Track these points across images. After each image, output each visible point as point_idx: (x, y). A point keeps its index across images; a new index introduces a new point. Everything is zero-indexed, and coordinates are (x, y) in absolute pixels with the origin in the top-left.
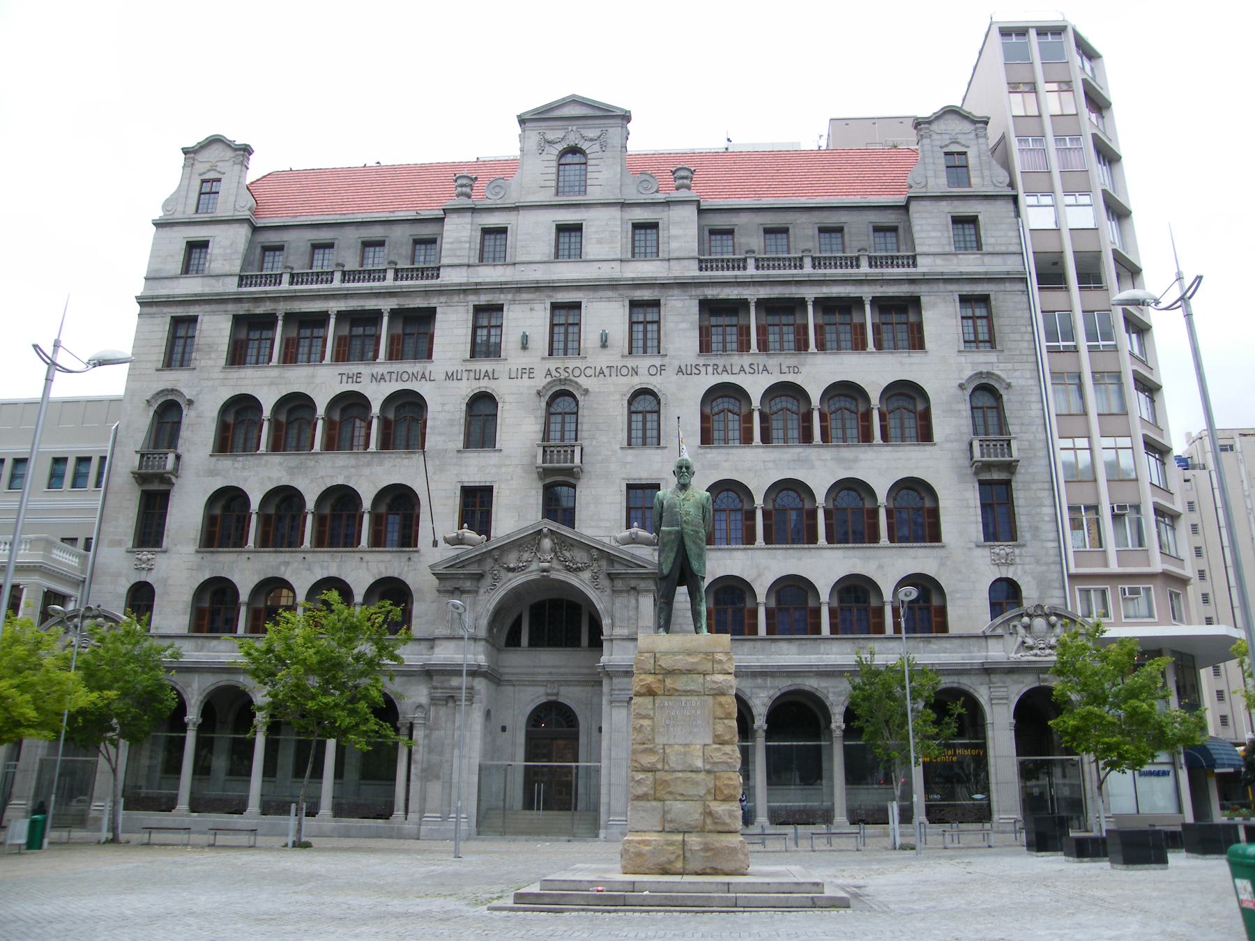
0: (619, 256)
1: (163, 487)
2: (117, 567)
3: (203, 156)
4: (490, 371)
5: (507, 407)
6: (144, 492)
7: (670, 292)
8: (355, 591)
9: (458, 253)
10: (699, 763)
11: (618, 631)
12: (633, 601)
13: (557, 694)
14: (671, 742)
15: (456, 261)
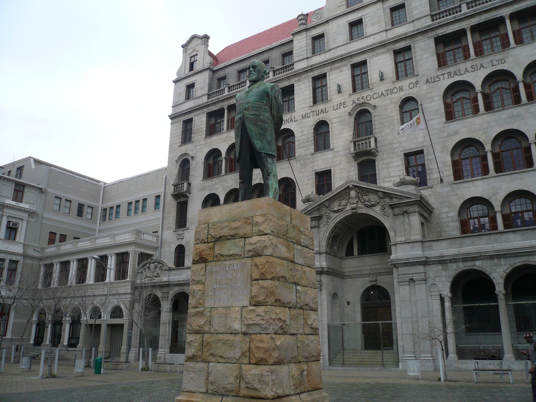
0: (384, 29)
1: (184, 200)
2: (171, 238)
3: (189, 47)
4: (323, 108)
5: (334, 125)
6: (178, 203)
7: (416, 39)
8: (494, 204)
9: (302, 53)
10: (237, 326)
11: (399, 239)
12: (407, 219)
13: (376, 281)
14: (217, 305)
15: (301, 58)
